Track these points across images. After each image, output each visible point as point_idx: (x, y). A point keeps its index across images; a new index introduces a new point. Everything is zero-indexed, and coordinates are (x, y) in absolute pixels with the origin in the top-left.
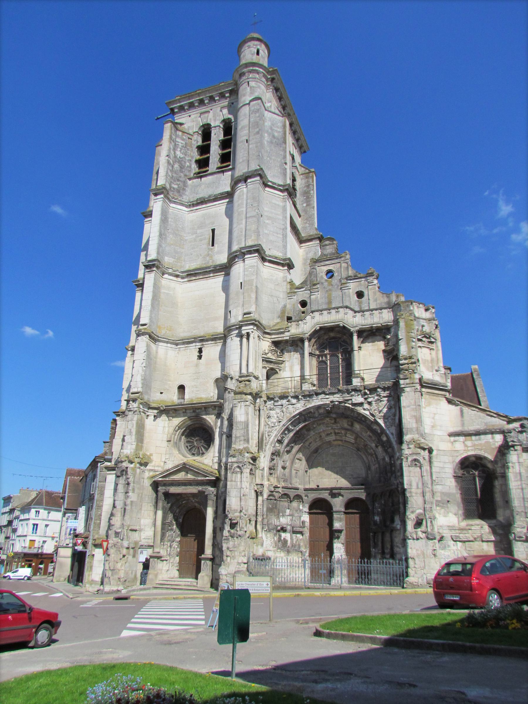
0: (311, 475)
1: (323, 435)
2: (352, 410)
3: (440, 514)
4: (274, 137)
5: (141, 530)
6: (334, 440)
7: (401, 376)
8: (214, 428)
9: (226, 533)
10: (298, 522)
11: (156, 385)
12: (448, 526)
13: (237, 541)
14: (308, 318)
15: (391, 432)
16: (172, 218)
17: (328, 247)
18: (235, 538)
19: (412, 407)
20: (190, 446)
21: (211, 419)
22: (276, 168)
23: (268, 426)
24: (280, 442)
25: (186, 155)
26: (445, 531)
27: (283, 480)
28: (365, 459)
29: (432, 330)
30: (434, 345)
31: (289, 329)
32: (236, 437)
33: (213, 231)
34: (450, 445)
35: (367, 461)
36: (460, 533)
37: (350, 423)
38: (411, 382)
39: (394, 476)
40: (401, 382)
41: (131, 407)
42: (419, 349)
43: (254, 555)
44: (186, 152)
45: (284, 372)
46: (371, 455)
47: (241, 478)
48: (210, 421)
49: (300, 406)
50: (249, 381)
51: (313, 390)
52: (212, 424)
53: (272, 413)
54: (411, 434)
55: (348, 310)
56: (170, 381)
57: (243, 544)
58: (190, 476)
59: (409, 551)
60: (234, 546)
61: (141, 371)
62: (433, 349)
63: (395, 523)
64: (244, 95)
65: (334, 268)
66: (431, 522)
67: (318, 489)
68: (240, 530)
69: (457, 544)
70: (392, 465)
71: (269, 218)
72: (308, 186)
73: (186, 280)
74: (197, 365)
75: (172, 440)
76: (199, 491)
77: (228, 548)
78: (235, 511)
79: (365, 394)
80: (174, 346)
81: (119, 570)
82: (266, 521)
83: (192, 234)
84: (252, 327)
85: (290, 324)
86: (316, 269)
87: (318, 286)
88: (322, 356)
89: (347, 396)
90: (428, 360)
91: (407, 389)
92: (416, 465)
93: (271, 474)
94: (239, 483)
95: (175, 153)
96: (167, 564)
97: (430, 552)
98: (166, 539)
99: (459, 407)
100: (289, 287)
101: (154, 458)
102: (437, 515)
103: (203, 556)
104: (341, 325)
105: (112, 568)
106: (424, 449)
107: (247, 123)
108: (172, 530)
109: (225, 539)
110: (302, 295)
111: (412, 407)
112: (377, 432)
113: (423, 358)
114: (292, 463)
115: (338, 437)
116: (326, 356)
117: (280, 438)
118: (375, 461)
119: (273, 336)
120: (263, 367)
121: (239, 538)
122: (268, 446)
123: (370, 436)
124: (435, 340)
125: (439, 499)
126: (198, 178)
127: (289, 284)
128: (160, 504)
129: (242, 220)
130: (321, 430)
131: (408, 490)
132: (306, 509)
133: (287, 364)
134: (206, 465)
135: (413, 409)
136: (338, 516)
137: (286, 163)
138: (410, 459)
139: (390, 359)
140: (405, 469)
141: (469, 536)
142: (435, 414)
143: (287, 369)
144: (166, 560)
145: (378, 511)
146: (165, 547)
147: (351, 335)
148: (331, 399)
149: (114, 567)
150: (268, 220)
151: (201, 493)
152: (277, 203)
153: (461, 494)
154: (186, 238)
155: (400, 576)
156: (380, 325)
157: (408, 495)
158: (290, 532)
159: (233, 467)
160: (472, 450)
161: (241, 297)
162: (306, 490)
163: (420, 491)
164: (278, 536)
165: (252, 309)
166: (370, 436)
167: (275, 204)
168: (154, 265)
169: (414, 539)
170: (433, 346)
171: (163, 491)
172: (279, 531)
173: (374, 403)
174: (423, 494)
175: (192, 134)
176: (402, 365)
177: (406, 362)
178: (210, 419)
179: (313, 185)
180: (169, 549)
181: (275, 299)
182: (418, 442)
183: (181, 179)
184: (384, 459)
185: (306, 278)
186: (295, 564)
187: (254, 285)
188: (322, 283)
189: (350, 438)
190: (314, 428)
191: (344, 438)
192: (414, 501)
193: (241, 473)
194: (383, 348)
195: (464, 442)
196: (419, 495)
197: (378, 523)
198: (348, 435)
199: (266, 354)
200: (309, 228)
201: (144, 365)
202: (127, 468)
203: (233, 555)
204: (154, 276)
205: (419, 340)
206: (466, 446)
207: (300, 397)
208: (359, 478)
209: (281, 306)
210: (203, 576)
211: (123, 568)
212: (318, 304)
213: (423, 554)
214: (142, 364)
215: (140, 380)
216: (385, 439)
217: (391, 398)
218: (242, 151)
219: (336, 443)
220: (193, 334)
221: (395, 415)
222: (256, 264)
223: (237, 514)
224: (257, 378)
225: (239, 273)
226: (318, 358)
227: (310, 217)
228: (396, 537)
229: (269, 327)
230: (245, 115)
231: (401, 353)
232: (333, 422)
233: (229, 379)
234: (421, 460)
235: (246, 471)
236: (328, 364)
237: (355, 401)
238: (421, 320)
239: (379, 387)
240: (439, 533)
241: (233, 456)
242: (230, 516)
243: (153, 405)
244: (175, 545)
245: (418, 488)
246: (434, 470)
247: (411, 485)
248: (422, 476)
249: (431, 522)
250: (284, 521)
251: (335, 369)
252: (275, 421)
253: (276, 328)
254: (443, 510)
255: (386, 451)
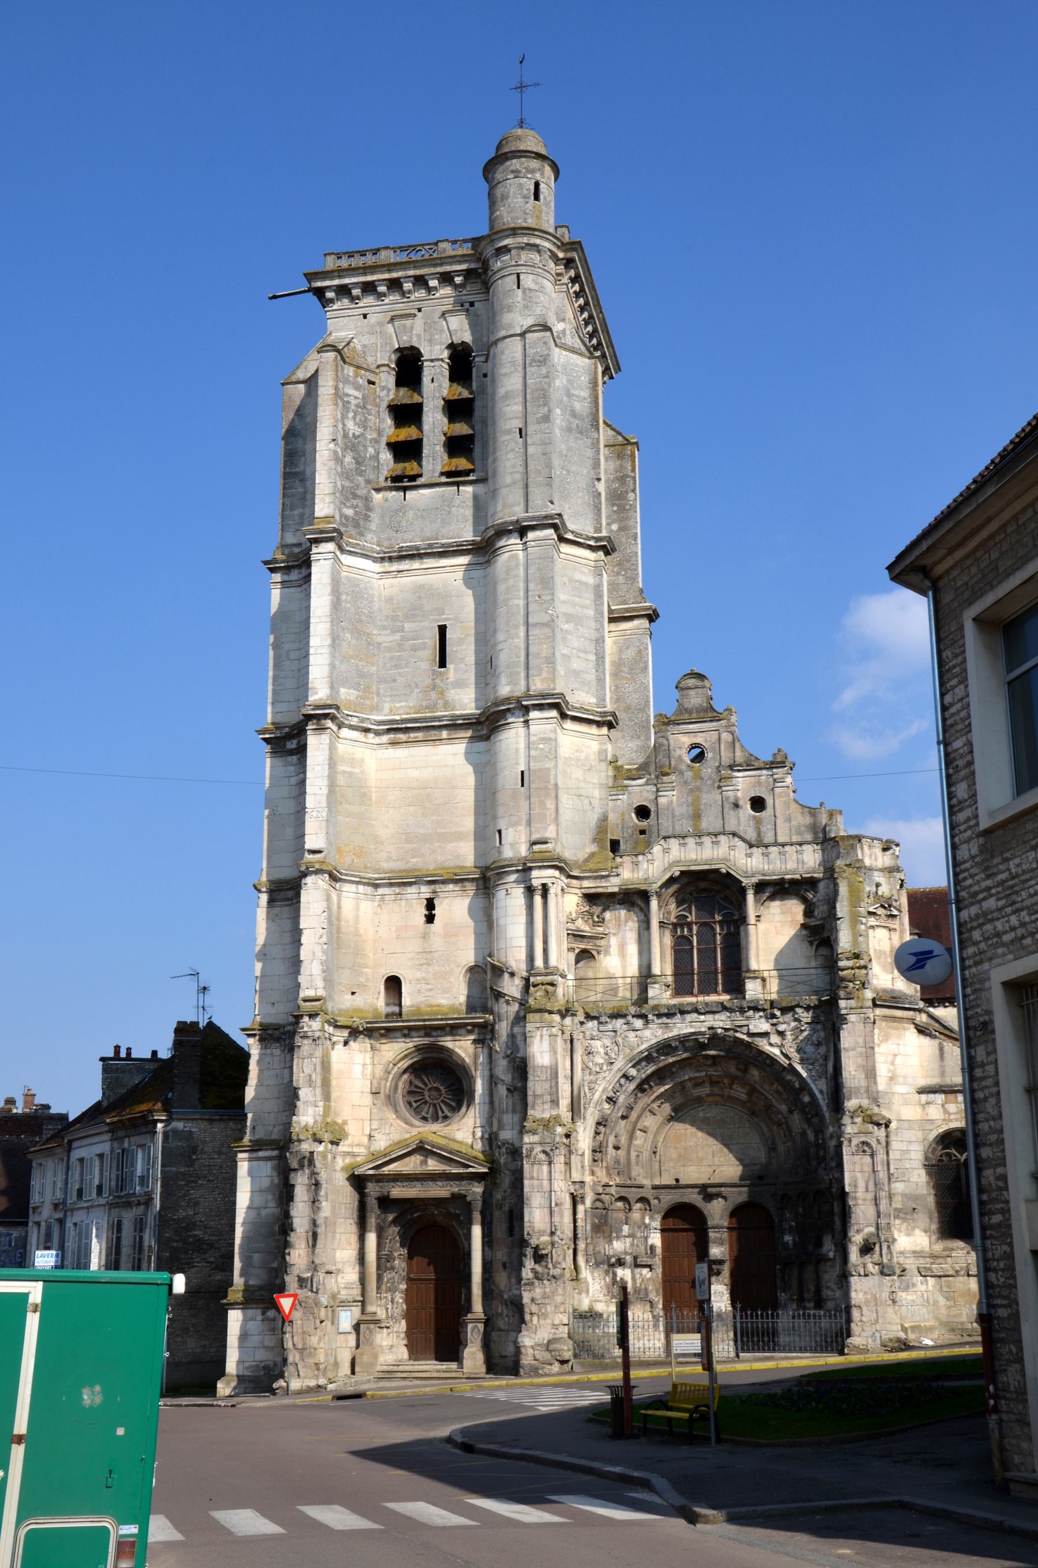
0: (663, 1158)
1: (689, 1085)
2: (748, 1045)
3: (900, 1231)
4: (574, 414)
5: (339, 1271)
6: (708, 1095)
7: (842, 993)
8: (473, 1069)
9: (527, 1273)
10: (643, 1248)
11: (344, 977)
12: (914, 1252)
13: (548, 1287)
14: (657, 849)
15: (819, 1088)
16: (348, 594)
17: (692, 692)
18: (545, 1282)
19: (859, 1049)
20: (416, 1102)
21: (465, 1051)
22: (581, 494)
23: (588, 1072)
24: (610, 1100)
25: (365, 428)
26: (907, 1261)
27: (616, 1171)
28: (766, 1130)
29: (895, 892)
30: (897, 921)
31: (620, 870)
32: (535, 1096)
33: (442, 630)
34: (919, 1109)
35: (768, 1135)
36: (932, 1263)
37: (741, 1066)
38: (860, 1005)
39: (823, 1165)
40: (842, 1003)
41: (305, 1029)
42: (871, 931)
43: (575, 1310)
44: (366, 420)
45: (608, 957)
46: (780, 1125)
47: (550, 1172)
48: (463, 1055)
49: (653, 1034)
50: (552, 984)
51: (675, 1005)
52: (467, 1060)
53: (597, 1045)
54: (856, 1098)
55: (736, 839)
56: (367, 967)
57: (560, 1291)
58: (433, 1165)
59: (853, 1294)
60: (545, 1296)
61: (319, 954)
62: (895, 930)
63: (825, 1249)
64: (510, 309)
65: (706, 741)
66: (889, 1247)
67: (677, 1186)
68: (555, 1267)
69: (927, 1281)
70: (821, 1146)
71: (569, 618)
72: (622, 479)
73: (385, 738)
74: (425, 936)
75: (382, 1091)
76: (452, 1194)
77: (533, 1300)
78: (542, 1233)
79: (773, 1016)
80: (369, 890)
81: (315, 1349)
82: (591, 1247)
83: (394, 631)
84: (557, 873)
85: (618, 860)
86: (668, 740)
87: (673, 777)
88: (682, 926)
89: (739, 1019)
90: (885, 952)
91: (852, 1018)
92: (864, 1151)
93: (595, 1161)
94: (546, 1183)
95: (344, 425)
96: (388, 1334)
97: (885, 1295)
98: (384, 1287)
99: (937, 1041)
100: (611, 773)
101: (350, 1128)
102: (896, 1235)
103: (469, 1316)
104: (724, 871)
105: (300, 1346)
106: (878, 1125)
107: (519, 386)
108: (392, 1268)
109: (525, 1284)
110: (640, 792)
111: (859, 1049)
112: (792, 1087)
113: (877, 948)
114: (631, 1137)
115: (716, 1090)
116: (689, 925)
117: (611, 1094)
118: (785, 1136)
119: (586, 884)
120: (569, 950)
121: (554, 1281)
122: (591, 1110)
123: (778, 1092)
124: (900, 911)
125: (899, 1206)
126: (397, 489)
127: (610, 768)
128: (372, 1221)
129: (517, 627)
130: (687, 1077)
131: (852, 1195)
132: (657, 1224)
133: (613, 941)
134: (461, 1143)
135: (861, 1053)
136: (718, 1235)
137: (599, 480)
138: (855, 1142)
139: (816, 943)
140: (846, 1158)
141: (947, 1267)
142: (895, 1055)
143: (614, 949)
144: (388, 1328)
145: (791, 1227)
146: (383, 1301)
147: (743, 891)
148: (708, 1024)
149: (304, 1344)
150: (567, 622)
151: (458, 1198)
152: (584, 579)
153: (936, 1195)
154: (380, 639)
155: (837, 1336)
156: (798, 877)
157: (851, 1203)
158: (630, 1267)
159: (534, 1153)
160: (956, 1120)
161: (524, 804)
162: (655, 1187)
163: (870, 1196)
164: (611, 1275)
165: (550, 833)
166: (778, 1092)
167: (580, 582)
168: (326, 716)
169: (860, 1275)
170: (895, 924)
171: (378, 1194)
172: (612, 1265)
173: (788, 1033)
174: (876, 1201)
175: (373, 367)
176: (843, 970)
177: (850, 963)
178: (463, 1047)
179: (634, 478)
180: (390, 1306)
181: (586, 802)
182: (869, 1112)
183: (359, 492)
184: (804, 1134)
185: (648, 757)
186: (640, 1324)
187: (552, 781)
188: (681, 773)
189: (740, 1093)
190: (673, 1073)
191: (726, 1092)
192: (861, 1214)
193: (550, 1163)
194: (800, 919)
195: (943, 1106)
196: (868, 1203)
197: (791, 1246)
198: (735, 1087)
199: (573, 921)
200: (624, 587)
201: (324, 939)
202: (312, 1153)
203: (543, 1311)
204: (328, 741)
205: (871, 913)
206: (946, 1112)
207: (650, 1017)
208: (754, 1165)
209: (596, 817)
210: (473, 1353)
211: (322, 1345)
212: (673, 816)
213: (876, 1299)
214: (321, 937)
215: (320, 972)
216: (806, 1099)
217: (819, 1026)
218: (511, 456)
219: (711, 1099)
220: (409, 866)
221: (826, 1058)
222: (552, 736)
223: (546, 1238)
224: (563, 976)
225: (517, 750)
226: (674, 931)
227: (628, 561)
228: (825, 1272)
229: (577, 865)
230: (513, 363)
231: (841, 945)
232: (709, 1062)
233: (506, 976)
234: (874, 1144)
235: (559, 1160)
236: (695, 944)
237: (753, 1029)
238: (876, 873)
239: (798, 1006)
240: (898, 1263)
241: (534, 1132)
242: (534, 1242)
243: (342, 1021)
244: (399, 1298)
245: (867, 1190)
246: (891, 1156)
247: (856, 1186)
248: (874, 1171)
249: (889, 1247)
250: (618, 1246)
251: (708, 954)
252: (601, 1061)
253: (591, 865)
254: (905, 1224)
255: (808, 1121)
